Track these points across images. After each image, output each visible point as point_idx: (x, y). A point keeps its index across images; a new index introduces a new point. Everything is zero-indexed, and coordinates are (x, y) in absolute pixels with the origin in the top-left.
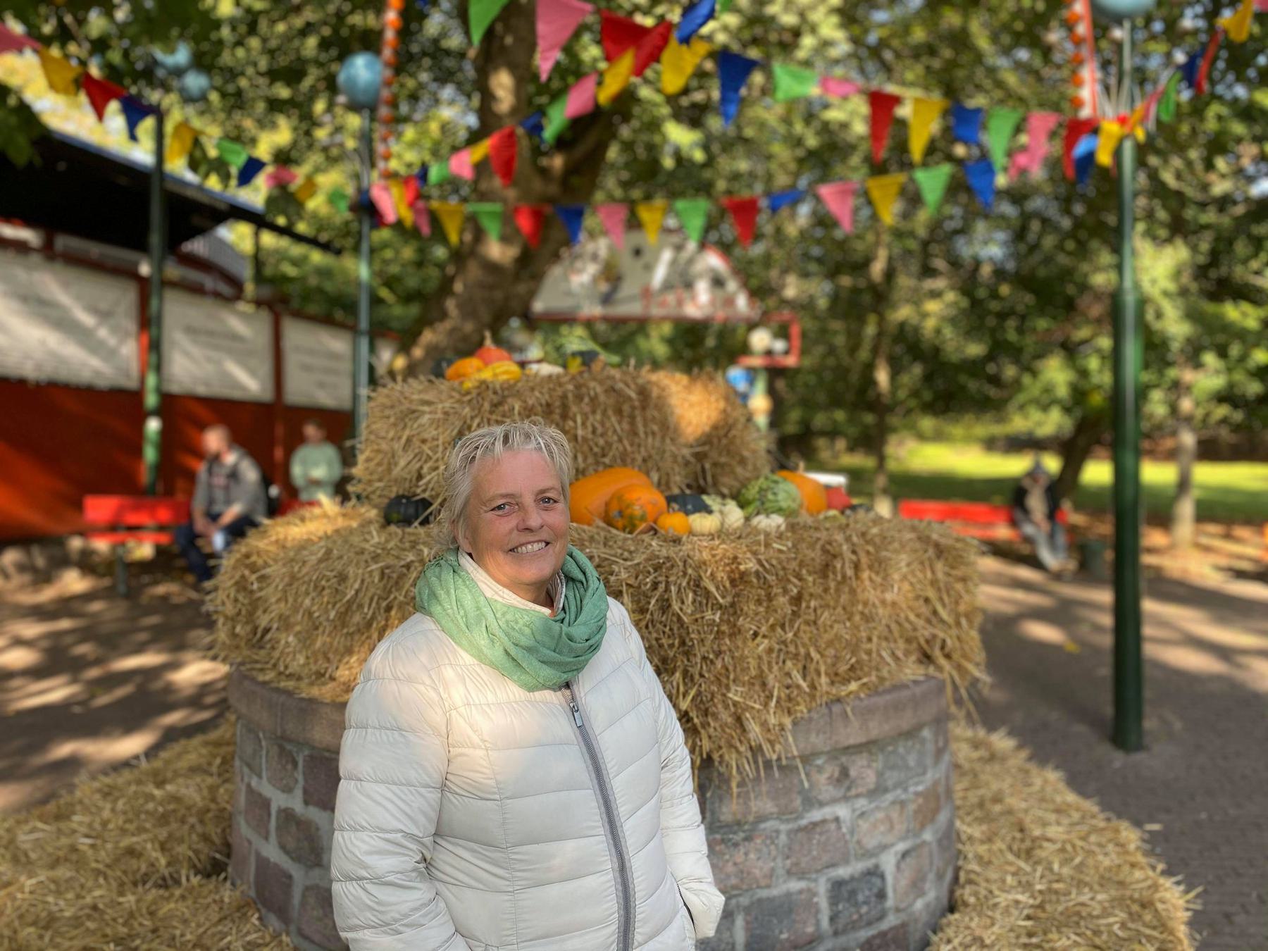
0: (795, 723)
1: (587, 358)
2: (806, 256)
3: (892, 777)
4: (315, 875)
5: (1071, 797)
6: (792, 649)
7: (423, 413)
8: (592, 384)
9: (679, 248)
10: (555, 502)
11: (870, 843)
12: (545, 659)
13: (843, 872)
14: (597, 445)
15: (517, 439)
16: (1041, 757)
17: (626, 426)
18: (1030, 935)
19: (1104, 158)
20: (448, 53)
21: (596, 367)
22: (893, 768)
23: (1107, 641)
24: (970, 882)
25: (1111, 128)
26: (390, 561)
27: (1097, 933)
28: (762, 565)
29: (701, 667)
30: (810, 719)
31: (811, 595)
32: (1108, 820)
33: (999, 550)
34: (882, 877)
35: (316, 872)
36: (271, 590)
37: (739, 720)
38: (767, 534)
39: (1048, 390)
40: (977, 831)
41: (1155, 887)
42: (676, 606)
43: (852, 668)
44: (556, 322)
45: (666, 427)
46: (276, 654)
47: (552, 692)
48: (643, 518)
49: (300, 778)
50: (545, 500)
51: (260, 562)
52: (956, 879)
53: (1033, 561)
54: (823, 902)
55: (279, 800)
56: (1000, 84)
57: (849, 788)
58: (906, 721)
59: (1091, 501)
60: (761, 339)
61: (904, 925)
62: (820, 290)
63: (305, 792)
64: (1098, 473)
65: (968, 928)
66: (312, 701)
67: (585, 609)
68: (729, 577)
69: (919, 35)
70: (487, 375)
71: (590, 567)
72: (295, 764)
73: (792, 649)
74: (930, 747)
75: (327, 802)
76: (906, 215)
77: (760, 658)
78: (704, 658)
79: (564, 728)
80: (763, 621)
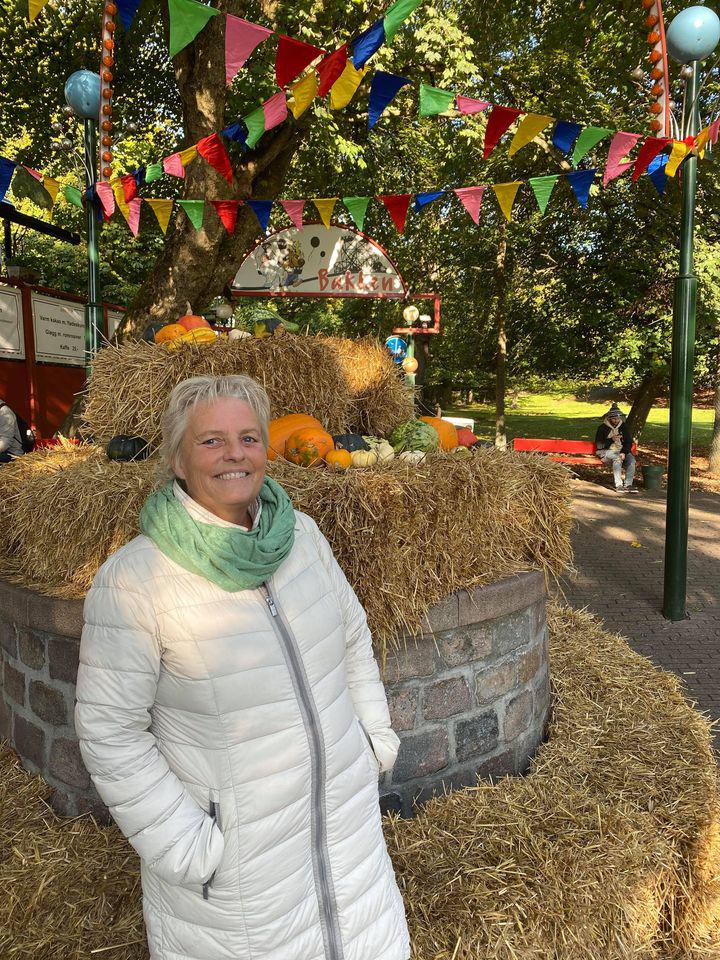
0: (430, 608)
1: (271, 325)
2: (445, 247)
3: (504, 646)
4: (62, 731)
5: (633, 655)
6: (429, 553)
7: (137, 369)
8: (275, 347)
9: (347, 240)
10: (255, 441)
11: (487, 694)
12: (243, 567)
13: (466, 716)
14: (279, 396)
15: (226, 388)
16: (611, 627)
17: (302, 381)
18: (601, 756)
19: (671, 172)
20: (159, 74)
21: (278, 333)
22: (504, 639)
23: (661, 540)
24: (559, 719)
25: (680, 148)
26: (113, 489)
27: (649, 752)
28: (407, 490)
29: (360, 569)
30: (443, 605)
31: (444, 512)
32: (659, 670)
33: (582, 473)
34: (496, 718)
35: (62, 730)
36: (17, 512)
37: (388, 607)
38: (411, 466)
39: (624, 353)
40: (565, 682)
41: (691, 718)
42: (340, 523)
43: (475, 565)
44: (258, 296)
45: (336, 382)
46: (24, 562)
47: (251, 592)
48: (315, 454)
49: (47, 659)
50: (246, 439)
51: (10, 490)
52: (550, 716)
53: (608, 482)
54: (452, 739)
55: (30, 675)
56: (597, 113)
57: (471, 655)
58: (514, 604)
59: (654, 436)
60: (411, 313)
61: (511, 752)
62: (456, 274)
63: (51, 668)
64: (659, 415)
65: (557, 752)
66: (54, 598)
67: (273, 528)
68: (381, 500)
69: (535, 70)
70: (188, 338)
71: (281, 492)
72: (42, 648)
73: (429, 553)
74: (532, 622)
75: (71, 678)
76: (521, 218)
77: (404, 560)
78: (361, 561)
79: (262, 618)
80: (407, 532)
